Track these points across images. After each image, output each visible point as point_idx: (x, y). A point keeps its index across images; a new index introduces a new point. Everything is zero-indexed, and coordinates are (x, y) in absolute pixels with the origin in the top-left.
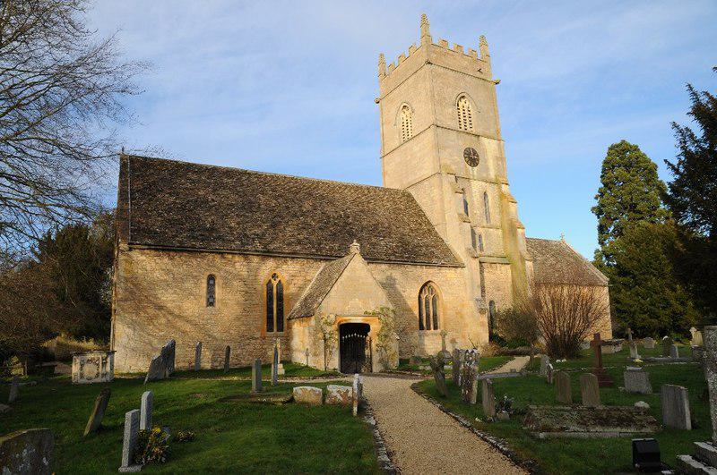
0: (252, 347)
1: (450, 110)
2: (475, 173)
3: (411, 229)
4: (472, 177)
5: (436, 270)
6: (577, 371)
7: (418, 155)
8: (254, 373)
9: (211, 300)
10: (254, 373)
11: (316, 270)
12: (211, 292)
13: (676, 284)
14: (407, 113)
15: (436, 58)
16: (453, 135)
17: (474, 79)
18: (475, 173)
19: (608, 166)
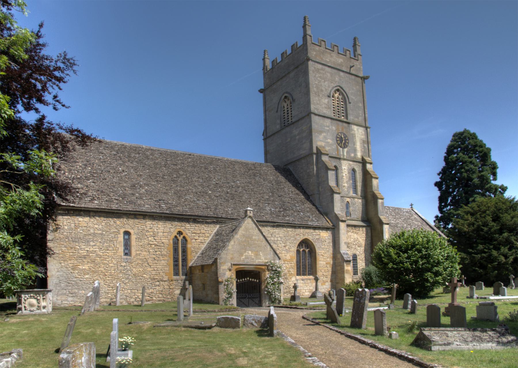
2: (345, 154)
6: (19, 290)
7: (297, 137)
8: (192, 310)
10: (192, 310)
11: (386, 228)
12: (127, 246)
14: (288, 102)
16: (328, 122)
18: (345, 154)
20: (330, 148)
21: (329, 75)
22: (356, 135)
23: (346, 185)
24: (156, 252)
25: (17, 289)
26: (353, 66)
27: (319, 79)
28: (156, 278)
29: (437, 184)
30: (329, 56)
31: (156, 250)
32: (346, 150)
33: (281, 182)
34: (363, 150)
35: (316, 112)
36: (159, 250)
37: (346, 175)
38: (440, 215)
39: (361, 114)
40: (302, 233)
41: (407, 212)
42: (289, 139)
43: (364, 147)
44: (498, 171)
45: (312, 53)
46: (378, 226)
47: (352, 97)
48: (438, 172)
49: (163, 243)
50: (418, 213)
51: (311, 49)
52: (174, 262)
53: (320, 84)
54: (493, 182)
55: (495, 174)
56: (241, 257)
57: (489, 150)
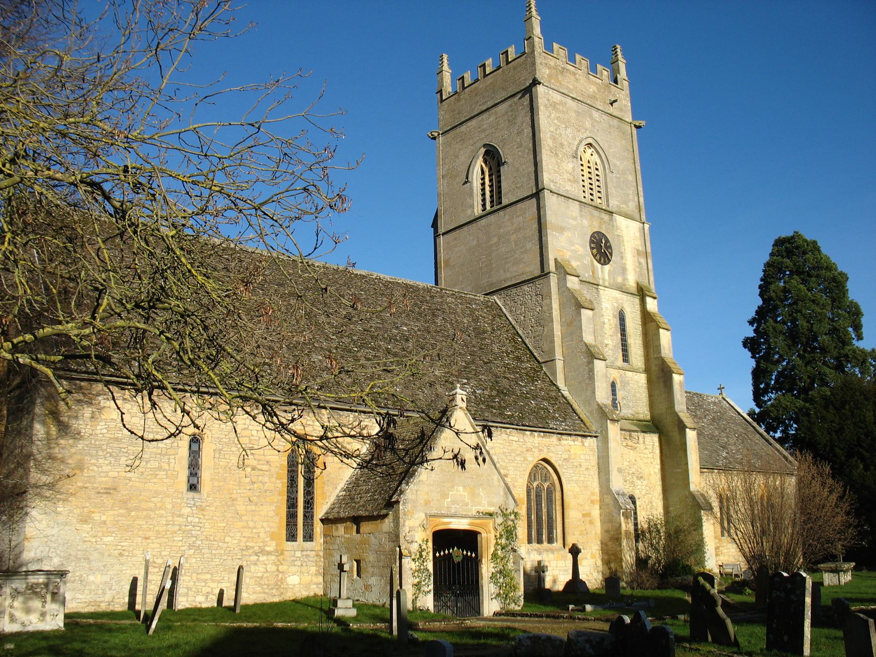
0: (261, 568)
1: (570, 165)
2: (607, 277)
3: (506, 366)
4: (601, 283)
5: (554, 438)
9: (194, 480)
13: (782, 431)
15: (550, 76)
17: (605, 117)
19: (771, 273)
20: (578, 263)
21: (573, 115)
22: (625, 239)
23: (610, 342)
24: (253, 483)
25: (771, 570)
26: (615, 101)
27: (556, 121)
28: (250, 544)
29: (749, 343)
30: (572, 77)
31: (254, 479)
32: (607, 267)
33: (484, 332)
34: (638, 270)
35: (553, 188)
36: (260, 478)
37: (609, 320)
38: (757, 410)
39: (631, 197)
40: (535, 447)
41: (715, 403)
42: (495, 240)
43: (640, 263)
44: (864, 320)
45: (544, 70)
46: (675, 434)
47: (615, 161)
48: (750, 317)
49: (267, 462)
50: (736, 408)
51: (541, 64)
52: (289, 508)
53: (557, 132)
54: (857, 344)
55: (857, 327)
56: (445, 499)
57: (844, 277)
